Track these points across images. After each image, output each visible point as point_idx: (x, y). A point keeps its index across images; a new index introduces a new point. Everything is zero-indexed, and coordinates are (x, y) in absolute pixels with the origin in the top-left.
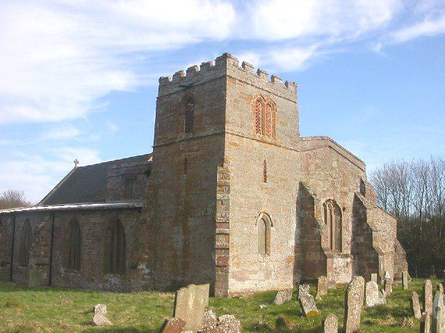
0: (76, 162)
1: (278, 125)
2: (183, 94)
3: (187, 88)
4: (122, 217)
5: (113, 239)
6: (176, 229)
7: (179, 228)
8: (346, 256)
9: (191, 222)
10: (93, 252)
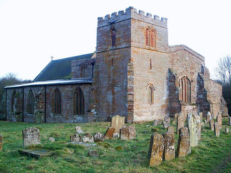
0: (52, 57)
1: (157, 41)
2: (110, 27)
3: (112, 23)
4: (82, 87)
5: (77, 98)
6: (109, 92)
7: (111, 92)
8: (193, 105)
9: (116, 89)
10: (67, 105)
